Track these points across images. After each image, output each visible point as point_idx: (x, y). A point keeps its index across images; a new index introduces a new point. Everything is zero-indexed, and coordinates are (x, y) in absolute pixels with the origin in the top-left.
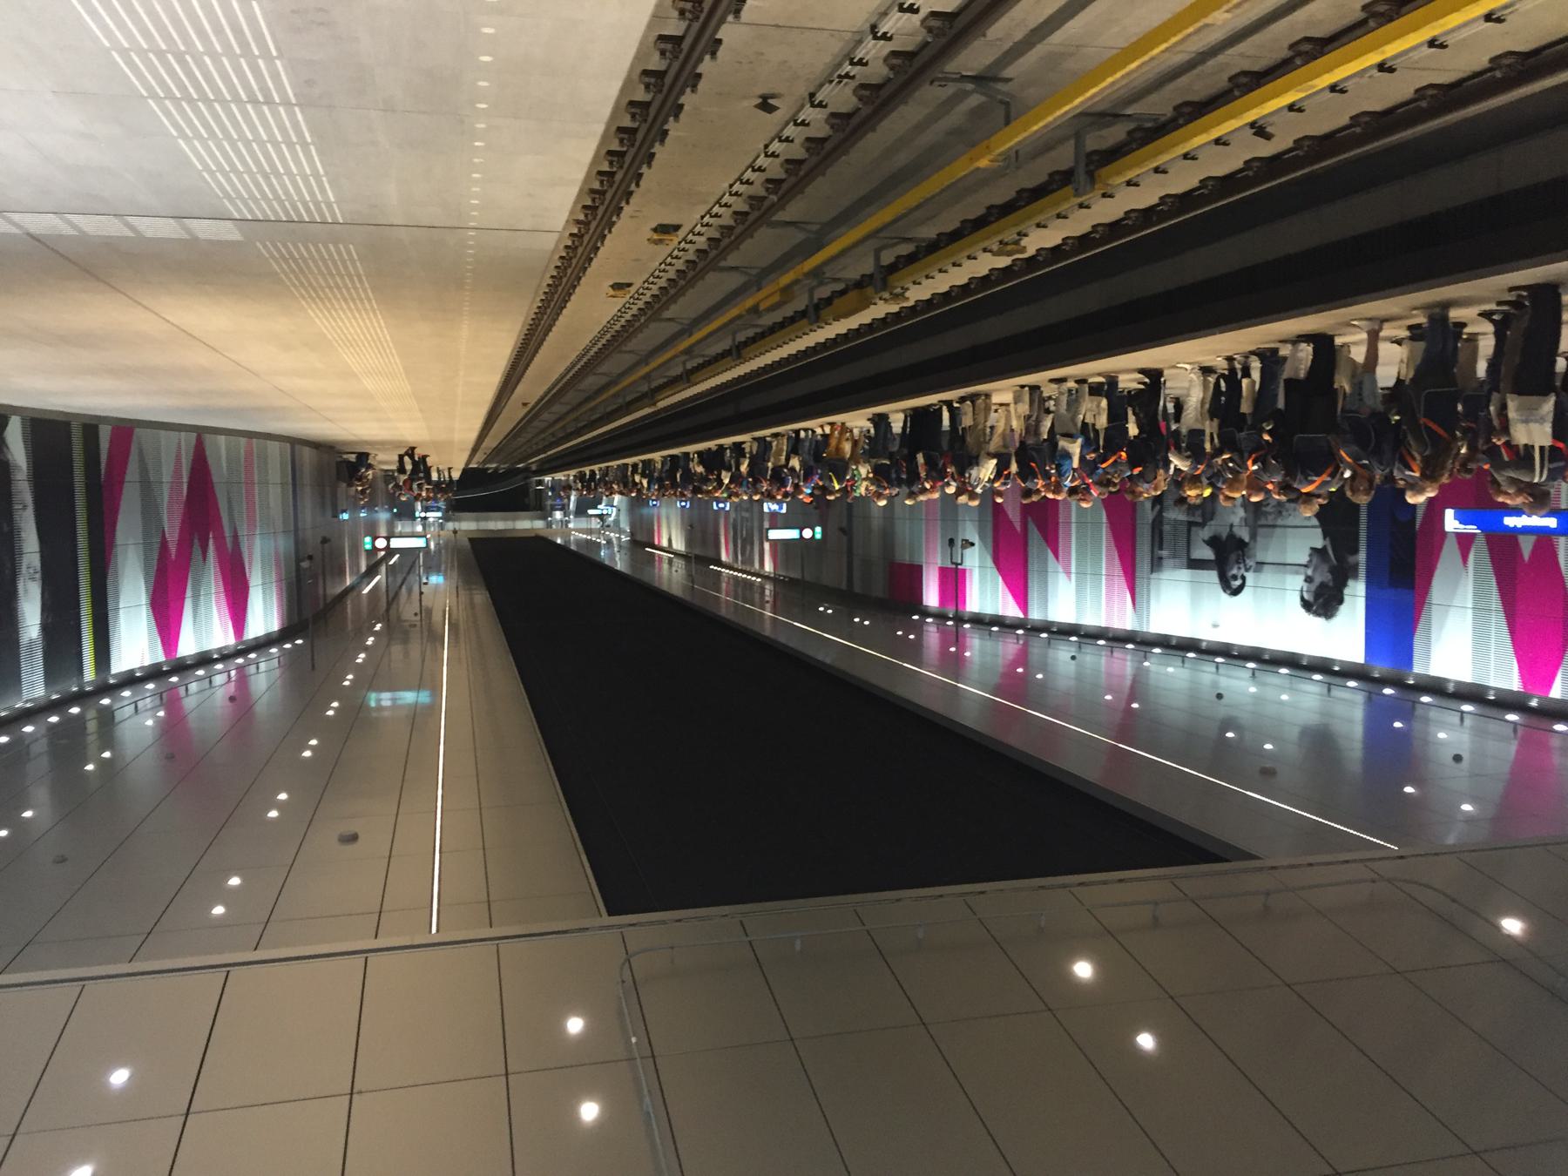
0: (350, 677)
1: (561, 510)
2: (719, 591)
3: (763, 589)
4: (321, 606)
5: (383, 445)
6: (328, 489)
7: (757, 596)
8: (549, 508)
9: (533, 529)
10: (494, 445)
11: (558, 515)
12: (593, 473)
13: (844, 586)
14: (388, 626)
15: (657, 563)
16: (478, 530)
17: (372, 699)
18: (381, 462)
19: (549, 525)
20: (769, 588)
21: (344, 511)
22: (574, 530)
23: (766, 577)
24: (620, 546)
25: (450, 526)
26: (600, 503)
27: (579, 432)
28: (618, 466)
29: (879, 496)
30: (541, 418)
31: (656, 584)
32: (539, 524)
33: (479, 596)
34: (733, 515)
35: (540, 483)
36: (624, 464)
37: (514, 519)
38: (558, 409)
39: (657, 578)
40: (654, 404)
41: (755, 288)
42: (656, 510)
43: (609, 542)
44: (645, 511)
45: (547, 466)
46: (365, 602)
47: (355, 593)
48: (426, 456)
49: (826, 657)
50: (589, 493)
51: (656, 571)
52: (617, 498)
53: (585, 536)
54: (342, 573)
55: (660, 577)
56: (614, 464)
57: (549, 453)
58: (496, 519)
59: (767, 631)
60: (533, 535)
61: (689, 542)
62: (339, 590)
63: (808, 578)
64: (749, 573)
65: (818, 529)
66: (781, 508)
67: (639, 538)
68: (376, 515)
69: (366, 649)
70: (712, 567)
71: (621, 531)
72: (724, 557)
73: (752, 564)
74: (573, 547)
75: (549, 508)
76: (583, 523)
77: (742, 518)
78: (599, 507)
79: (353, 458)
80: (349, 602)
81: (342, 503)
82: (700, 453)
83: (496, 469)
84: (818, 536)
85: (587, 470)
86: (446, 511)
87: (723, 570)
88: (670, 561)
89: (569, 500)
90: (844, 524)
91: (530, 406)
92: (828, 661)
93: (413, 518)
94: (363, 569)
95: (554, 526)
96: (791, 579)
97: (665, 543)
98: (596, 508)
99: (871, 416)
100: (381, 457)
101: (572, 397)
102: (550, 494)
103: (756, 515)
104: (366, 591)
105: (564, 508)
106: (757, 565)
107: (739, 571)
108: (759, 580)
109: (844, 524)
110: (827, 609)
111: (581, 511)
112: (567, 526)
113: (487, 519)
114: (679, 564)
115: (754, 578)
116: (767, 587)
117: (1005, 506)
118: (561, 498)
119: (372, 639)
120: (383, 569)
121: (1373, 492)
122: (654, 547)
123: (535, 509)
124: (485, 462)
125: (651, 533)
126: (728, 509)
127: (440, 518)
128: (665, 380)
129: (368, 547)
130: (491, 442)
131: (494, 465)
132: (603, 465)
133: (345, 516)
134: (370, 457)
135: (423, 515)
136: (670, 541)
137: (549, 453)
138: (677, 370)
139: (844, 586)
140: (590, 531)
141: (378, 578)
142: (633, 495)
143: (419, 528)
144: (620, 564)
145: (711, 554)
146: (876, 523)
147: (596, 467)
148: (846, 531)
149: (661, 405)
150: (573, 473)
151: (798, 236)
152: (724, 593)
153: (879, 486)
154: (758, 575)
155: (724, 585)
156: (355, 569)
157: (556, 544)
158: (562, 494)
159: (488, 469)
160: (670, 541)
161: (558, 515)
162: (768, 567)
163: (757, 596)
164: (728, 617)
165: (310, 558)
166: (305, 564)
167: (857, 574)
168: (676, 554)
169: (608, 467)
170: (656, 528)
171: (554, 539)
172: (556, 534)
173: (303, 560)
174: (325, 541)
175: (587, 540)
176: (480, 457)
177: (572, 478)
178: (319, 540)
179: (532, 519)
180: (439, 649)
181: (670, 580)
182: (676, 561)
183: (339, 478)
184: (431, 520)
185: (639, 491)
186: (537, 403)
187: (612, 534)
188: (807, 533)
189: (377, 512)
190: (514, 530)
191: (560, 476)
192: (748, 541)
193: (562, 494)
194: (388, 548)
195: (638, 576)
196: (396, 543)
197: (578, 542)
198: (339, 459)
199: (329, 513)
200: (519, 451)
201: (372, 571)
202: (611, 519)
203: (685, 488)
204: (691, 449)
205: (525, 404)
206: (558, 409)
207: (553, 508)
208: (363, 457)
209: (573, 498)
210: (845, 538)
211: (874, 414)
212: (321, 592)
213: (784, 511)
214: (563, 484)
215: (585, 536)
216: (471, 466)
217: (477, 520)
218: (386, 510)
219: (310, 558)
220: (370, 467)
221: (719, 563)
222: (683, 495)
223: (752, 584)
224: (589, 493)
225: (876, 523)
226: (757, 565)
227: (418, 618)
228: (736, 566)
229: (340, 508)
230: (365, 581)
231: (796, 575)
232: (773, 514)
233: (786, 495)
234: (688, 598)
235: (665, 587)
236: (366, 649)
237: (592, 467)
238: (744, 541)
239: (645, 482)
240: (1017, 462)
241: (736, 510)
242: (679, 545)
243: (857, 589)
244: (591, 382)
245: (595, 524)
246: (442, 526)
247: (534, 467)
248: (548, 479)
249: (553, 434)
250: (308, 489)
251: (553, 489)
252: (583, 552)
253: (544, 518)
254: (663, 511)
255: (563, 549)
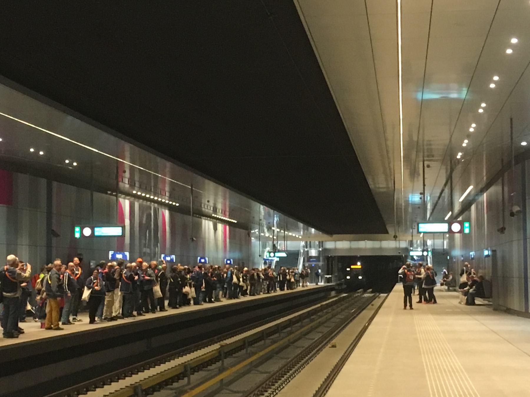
0: (483, 105)
1: (311, 257)
2: (132, 169)
3: (132, 184)
4: (506, 174)
5: (454, 312)
6: (500, 273)
7: (137, 178)
8: (321, 258)
9: (335, 241)
10: (364, 312)
11: (313, 253)
12: (282, 289)
13: (55, 184)
14: (452, 156)
15: (228, 209)
16: (381, 240)
17: (463, 94)
18: (457, 297)
19: (321, 244)
20: (125, 185)
21: (488, 256)
22: (301, 240)
23: (128, 194)
24: (260, 225)
25: (403, 244)
26: (277, 262)
27: (291, 323)
28: (259, 294)
29: (14, 264)
30: (321, 335)
31: (228, 191)
32: (330, 245)
33: (381, 186)
34: (158, 250)
35: (328, 280)
36: (254, 295)
37: (350, 249)
38: (306, 343)
39: (228, 196)
40: (222, 346)
41: (224, 382)
42: (228, 256)
43: (269, 228)
44: (237, 255)
45: (322, 294)
46: (473, 179)
47: (480, 186)
48: (418, 302)
49: (70, 120)
50: (284, 270)
51: (228, 203)
52: (262, 267)
53: (290, 234)
54: (490, 204)
55: (225, 199)
56: (262, 296)
57: (319, 305)
58: (365, 250)
59: (127, 147)
60: (335, 236)
61: (198, 227)
62: (492, 189)
63: (88, 192)
64: (145, 198)
65: (77, 235)
66: (113, 256)
67: (243, 232)
68: (463, 253)
69: (469, 136)
70: (236, 222)
71: (259, 238)
72: (167, 213)
73: (140, 206)
74: (301, 225)
75: (321, 258)
76: (292, 245)
77: (149, 247)
78: (278, 259)
79: (478, 301)
80: (485, 178)
81: (489, 263)
82: (188, 304)
83: (365, 291)
84: (77, 229)
85: (286, 291)
86: (407, 257)
87: (228, 220)
88: (215, 210)
89: (304, 265)
90: (54, 240)
91: (329, 345)
92: (70, 118)
93: (434, 252)
94: (473, 207)
95: (317, 243)
96: (107, 193)
97: (220, 226)
98: (280, 258)
99: (21, 336)
100: (456, 302)
101: (293, 353)
102: (320, 271)
103: (137, 248)
104: (471, 188)
105: (308, 258)
106: (137, 205)
107: (153, 201)
108: (134, 192)
109: (54, 240)
110: (71, 164)
111: (293, 257)
112: (306, 243)
113: (373, 249)
114: (208, 209)
115: (139, 193)
116: (127, 186)
117: (28, 261)
118: (311, 267)
119: (464, 145)
120: (457, 208)
121: (159, 282)
122: (230, 223)
123: (333, 258)
124: (373, 298)
125: (232, 236)
126: (163, 256)
127: (412, 250)
128: (209, 367)
129: (467, 224)
130: (366, 313)
131: (366, 295)
132: (273, 294)
133: (486, 253)
134: (465, 301)
135: (425, 253)
136: (215, 229)
137: (319, 305)
138: (195, 377)
139: (55, 184)
140: (285, 238)
141: (461, 199)
142: (246, 269)
143: (429, 242)
144: (262, 210)
145: (179, 217)
146: (24, 241)
147: (279, 292)
148: (51, 233)
149: (216, 346)
150: (300, 289)
151: (232, 387)
152: (167, 181)
153: (13, 273)
154: (136, 196)
155: (167, 189)
156: (480, 207)
157: (316, 228)
158: (309, 271)
159: (372, 292)
160: (215, 229)
161: (313, 253)
162: (126, 204)
163: (137, 178)
164: (164, 161)
165: (512, 214)
166: (516, 209)
167: (43, 192)
168: (209, 217)
169: (268, 293)
170: (228, 240)
171: (317, 232)
172: (315, 236)
173: (518, 212)
174: (502, 230)
175: (288, 230)
176: (377, 302)
177: (301, 284)
178: (506, 231)
179: (335, 249)
180: (410, 136)
181: (216, 195)
182: (210, 211)
183: (490, 284)
184: (419, 249)
185: (240, 270)
186: (324, 346)
187: (267, 235)
188: (87, 232)
189: (462, 256)
190: (350, 240)
191: (310, 286)
192: (144, 227)
193: (309, 271)
194: (450, 224)
195: (244, 199)
196: (443, 227)
197: (296, 229)
198: (491, 300)
199: (499, 254)
200: (343, 307)
201: (466, 207)
202: (268, 249)
203: (198, 274)
204: (192, 308)
205: (334, 346)
206: (306, 343)
207: (317, 258)
208: (470, 302)
209: (300, 267)
210: (54, 228)
211: (17, 337)
212: (506, 189)
213: (111, 253)
214: (308, 279)
215: (290, 234)
216: (386, 295)
217: (381, 249)
218: (455, 257)
219: (512, 214)
220: (466, 294)
221: (171, 208)
222: (200, 268)
223: (141, 188)
224: (284, 270)
225: (24, 241)
226: (137, 205)
227: (426, 163)
228: (156, 205)
229: (490, 258)
230: (471, 198)
231: (97, 196)
232: (121, 249)
233: (103, 266)
234: (199, 178)
235: (221, 189)
236: (469, 136)
237: (282, 293)
238: (148, 227)
239: (235, 280)
240: (428, 293)
241: (155, 254)
242: (207, 225)
243: (43, 182)
244: (273, 366)
245: (280, 245)
246: (411, 244)
247: (333, 293)
248: (322, 284)
249: (312, 321)
250: (515, 273)
251: (317, 275)
252: (291, 220)
253: (325, 250)
254: (221, 255)
255: (309, 223)
